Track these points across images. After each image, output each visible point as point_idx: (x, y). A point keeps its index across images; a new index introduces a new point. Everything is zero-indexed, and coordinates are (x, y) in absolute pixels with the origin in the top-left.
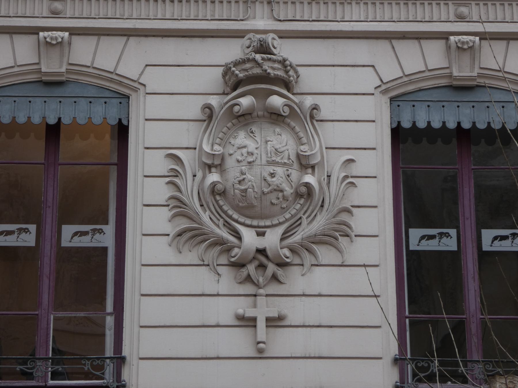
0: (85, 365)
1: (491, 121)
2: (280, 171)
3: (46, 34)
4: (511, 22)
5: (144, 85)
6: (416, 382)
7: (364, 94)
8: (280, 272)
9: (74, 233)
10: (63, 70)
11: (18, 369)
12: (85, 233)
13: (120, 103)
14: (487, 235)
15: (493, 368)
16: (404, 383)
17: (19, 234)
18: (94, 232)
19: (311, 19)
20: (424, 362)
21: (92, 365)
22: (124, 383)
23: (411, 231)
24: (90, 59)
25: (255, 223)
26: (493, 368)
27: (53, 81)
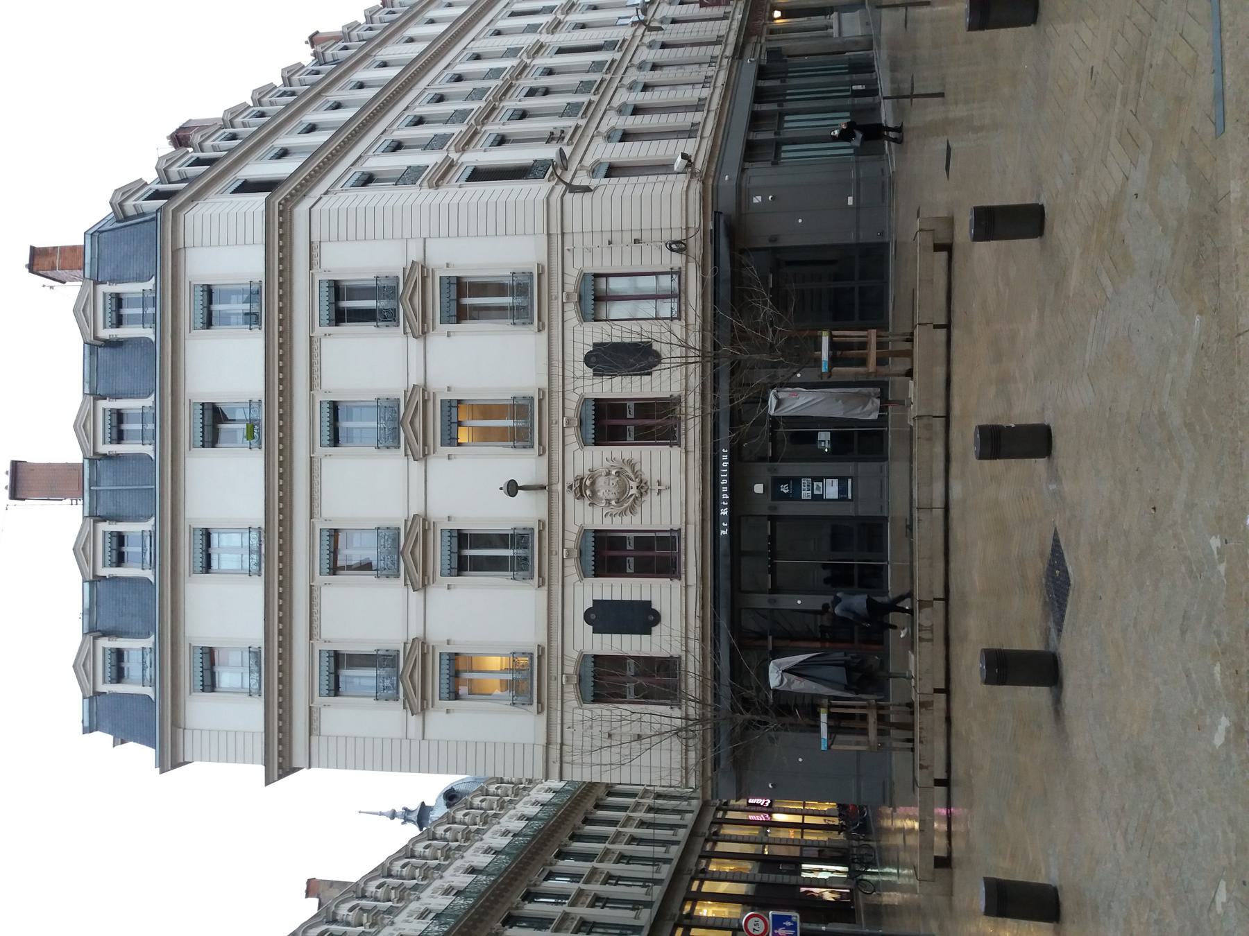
2: (611, 482)
8: (644, 482)
23: (628, 417)
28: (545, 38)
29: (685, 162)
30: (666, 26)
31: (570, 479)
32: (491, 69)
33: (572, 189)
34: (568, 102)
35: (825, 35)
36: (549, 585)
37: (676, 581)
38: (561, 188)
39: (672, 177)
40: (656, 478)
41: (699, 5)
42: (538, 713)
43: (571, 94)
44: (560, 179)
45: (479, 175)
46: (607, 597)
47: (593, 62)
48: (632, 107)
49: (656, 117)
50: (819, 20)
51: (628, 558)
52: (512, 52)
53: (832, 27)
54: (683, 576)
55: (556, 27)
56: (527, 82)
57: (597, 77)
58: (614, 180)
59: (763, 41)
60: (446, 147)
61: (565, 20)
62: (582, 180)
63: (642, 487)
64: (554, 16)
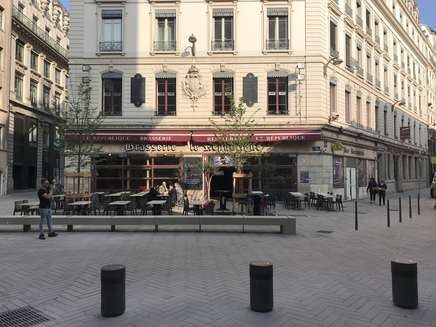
2: (197, 85)
7: (196, 2)
8: (197, 100)
25: (193, 93)
28: (392, 63)
29: (335, 117)
30: (394, 113)
31: (197, 67)
32: (380, 39)
33: (326, 67)
34: (364, 70)
35: (386, 177)
37: (266, 113)
38: (326, 62)
39: (329, 111)
40: (198, 105)
41: (401, 127)
42: (97, 54)
43: (367, 71)
44: (329, 62)
45: (333, 26)
47: (380, 82)
48: (360, 97)
49: (355, 106)
50: (392, 174)
52: (386, 48)
53: (389, 179)
54: (156, 117)
55: (396, 68)
56: (373, 53)
57: (374, 83)
58: (329, 86)
59: (385, 152)
60: (346, 14)
61: (398, 72)
62: (330, 72)
63: (194, 99)
64: (400, 68)
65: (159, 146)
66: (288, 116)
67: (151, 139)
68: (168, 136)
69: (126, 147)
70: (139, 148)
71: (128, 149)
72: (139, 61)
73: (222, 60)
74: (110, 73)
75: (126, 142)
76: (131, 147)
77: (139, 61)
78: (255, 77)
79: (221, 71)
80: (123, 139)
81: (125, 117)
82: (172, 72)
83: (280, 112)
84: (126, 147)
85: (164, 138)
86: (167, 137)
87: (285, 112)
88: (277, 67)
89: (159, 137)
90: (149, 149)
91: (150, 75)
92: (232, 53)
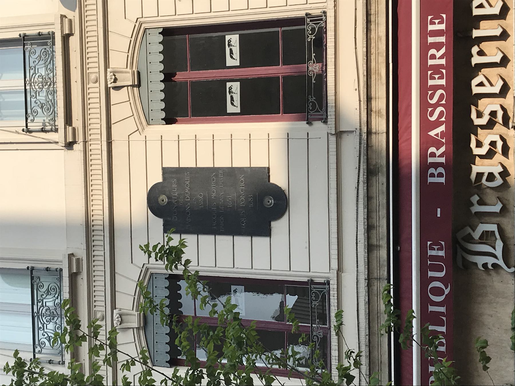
0: (315, 305)
1: (165, 351)
3: (109, 83)
4: (105, 287)
5: (144, 264)
6: (322, 111)
9: (231, 58)
10: (136, 313)
11: (319, 347)
12: (232, 98)
13: (149, 34)
14: (229, 62)
15: (312, 60)
16: (323, 118)
17: (232, 93)
18: (230, 45)
19: (105, 306)
20: (313, 296)
21: (311, 110)
22: (326, 282)
23: (229, 111)
24: (130, 297)
26: (312, 60)
27: (138, 81)
36: (85, 142)
37: (318, 125)
46: (187, 162)
51: (229, 84)
65: (481, 84)
66: (333, 286)
67: (442, 128)
68: (424, 33)
69: (485, 265)
70: (491, 197)
71: (495, 257)
72: (101, 218)
73: (96, 82)
74: (150, 328)
75: (460, 263)
76: (487, 237)
77: (101, 223)
78: (164, 178)
79: (139, 85)
80: (442, 274)
81: (335, 265)
82: (139, 53)
83: (310, 59)
84: (485, 265)
85: (433, 57)
86: (431, 40)
87: (313, 29)
88: (124, 80)
89: (431, 82)
90: (497, 138)
91: (154, 147)
92: (66, 38)
